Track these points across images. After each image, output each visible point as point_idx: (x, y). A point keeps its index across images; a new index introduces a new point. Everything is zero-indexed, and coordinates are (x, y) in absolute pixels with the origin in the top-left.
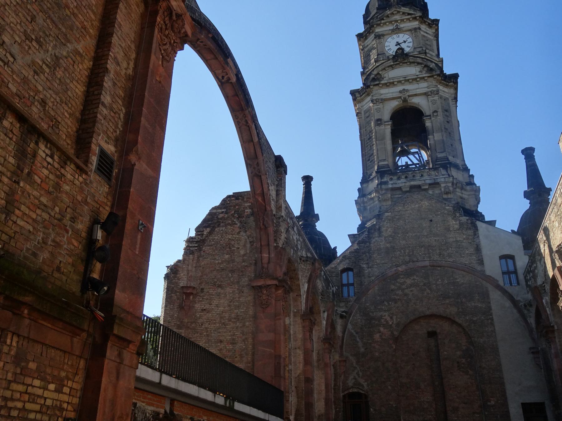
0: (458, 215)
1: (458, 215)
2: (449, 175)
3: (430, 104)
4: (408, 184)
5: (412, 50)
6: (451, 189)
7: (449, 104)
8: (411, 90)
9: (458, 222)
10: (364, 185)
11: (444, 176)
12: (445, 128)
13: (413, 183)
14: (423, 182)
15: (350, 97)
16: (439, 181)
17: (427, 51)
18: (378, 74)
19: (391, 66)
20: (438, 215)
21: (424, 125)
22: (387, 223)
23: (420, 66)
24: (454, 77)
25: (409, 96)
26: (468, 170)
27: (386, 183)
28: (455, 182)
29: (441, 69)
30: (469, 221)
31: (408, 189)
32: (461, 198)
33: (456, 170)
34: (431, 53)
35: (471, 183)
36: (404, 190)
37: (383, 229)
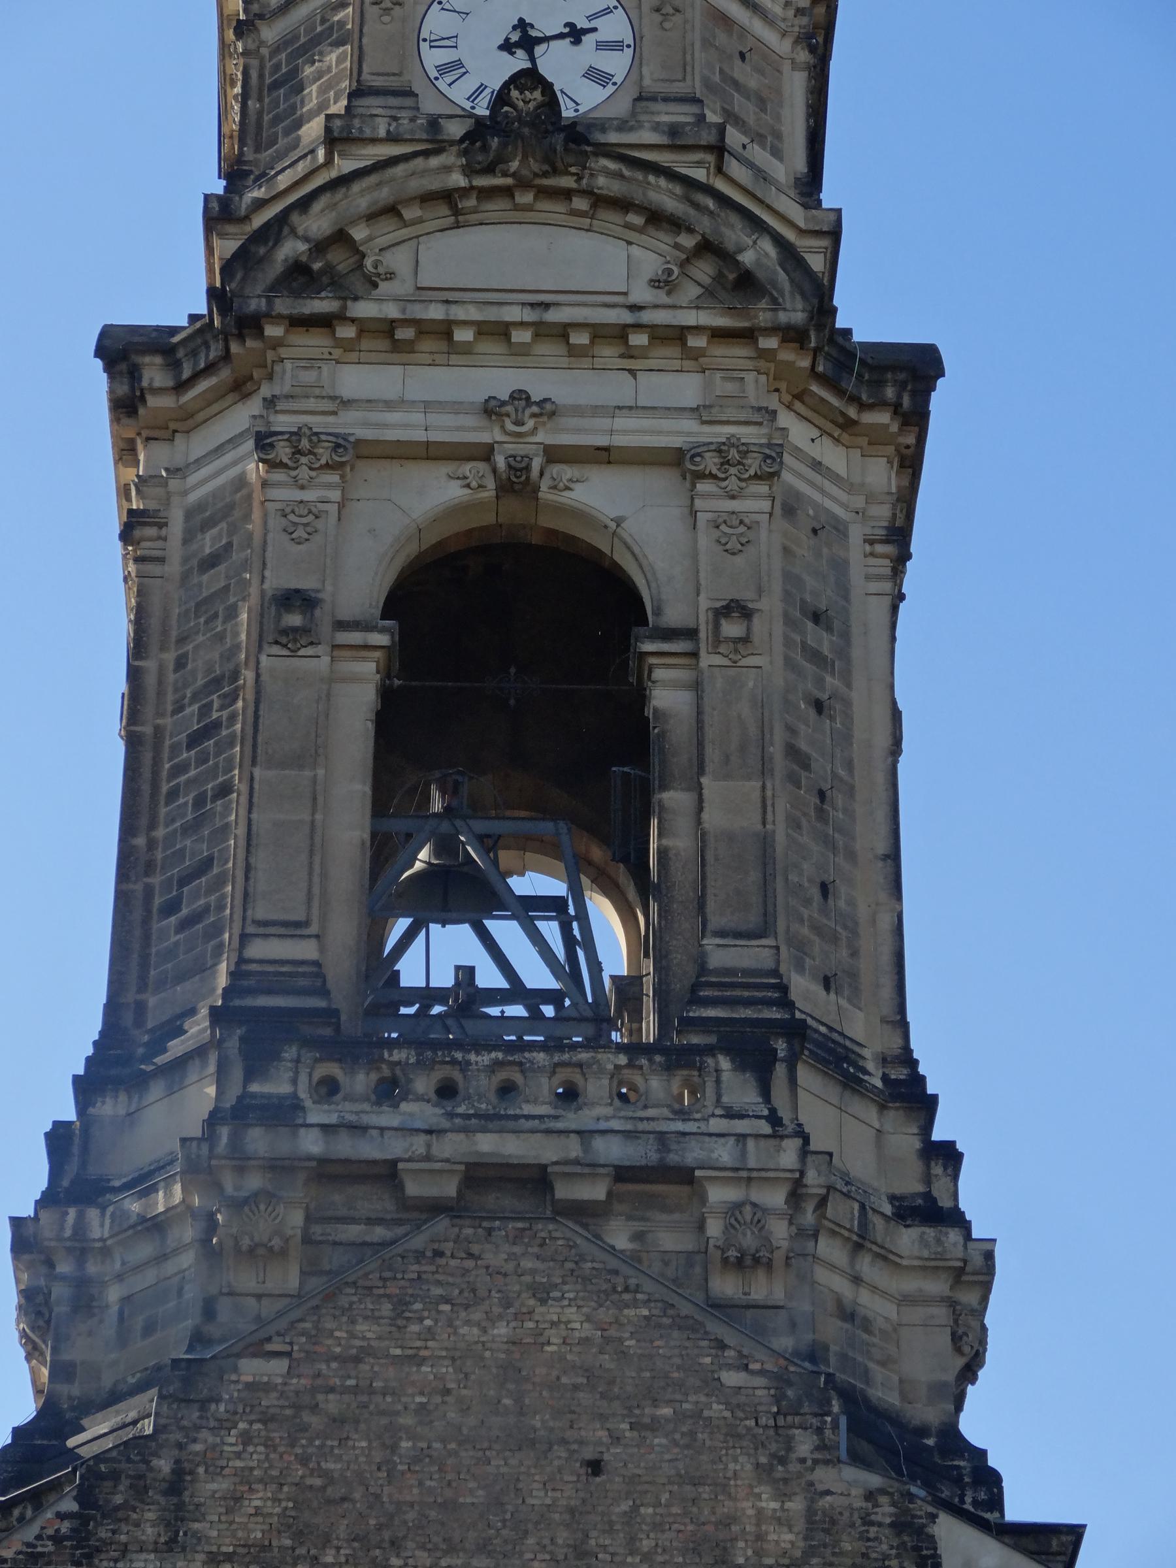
0: (804, 1445)
1: (804, 1445)
2: (774, 1119)
3: (704, 540)
4: (452, 1146)
5: (621, 108)
6: (780, 1231)
7: (841, 566)
8: (578, 411)
9: (796, 1505)
10: (108, 1108)
11: (741, 1126)
12: (792, 751)
13: (487, 1144)
14: (574, 1148)
15: (95, 383)
16: (692, 1154)
17: (734, 138)
18: (341, 237)
19: (448, 197)
20: (654, 1426)
21: (640, 697)
22: (246, 1439)
23: (662, 241)
24: (918, 368)
25: (553, 455)
26: (926, 1106)
27: (284, 1113)
28: (813, 1179)
29: (824, 310)
30: (885, 1511)
31: (449, 1189)
32: (848, 1314)
33: (833, 1092)
34: (759, 155)
35: (938, 1214)
36: (413, 1189)
37: (209, 1487)
